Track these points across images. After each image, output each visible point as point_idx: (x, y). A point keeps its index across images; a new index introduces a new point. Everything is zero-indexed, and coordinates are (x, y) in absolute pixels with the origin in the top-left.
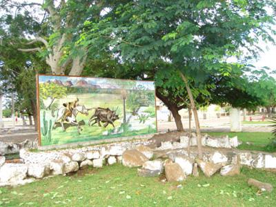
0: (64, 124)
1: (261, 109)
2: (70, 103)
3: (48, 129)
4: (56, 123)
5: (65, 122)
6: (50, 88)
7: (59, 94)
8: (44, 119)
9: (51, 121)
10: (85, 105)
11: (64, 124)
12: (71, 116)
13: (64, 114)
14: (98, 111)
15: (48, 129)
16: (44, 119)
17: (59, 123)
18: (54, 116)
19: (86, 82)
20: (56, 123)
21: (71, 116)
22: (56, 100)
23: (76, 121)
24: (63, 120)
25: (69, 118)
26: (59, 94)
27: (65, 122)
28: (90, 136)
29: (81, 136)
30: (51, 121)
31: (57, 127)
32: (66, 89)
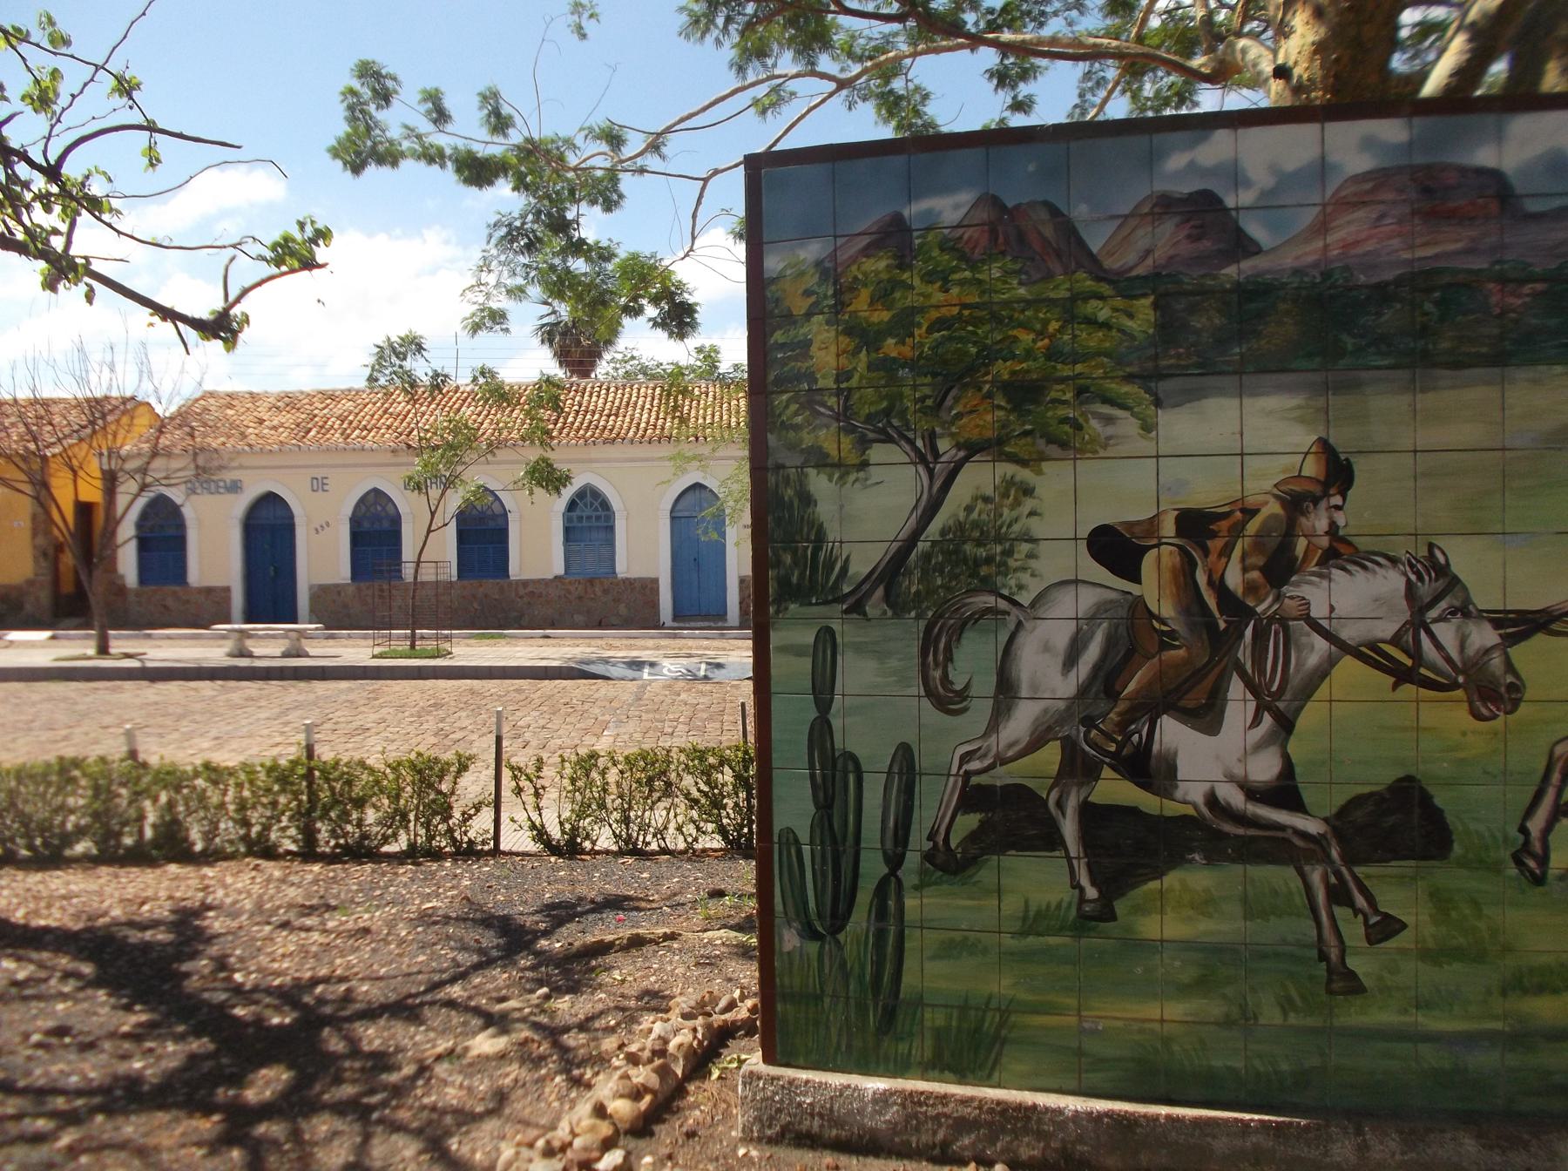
0: (1092, 815)
1: (478, 1156)
2: (1195, 524)
3: (873, 866)
4: (973, 797)
5: (1113, 789)
6: (903, 324)
7: (1023, 394)
8: (821, 730)
9: (905, 764)
10: (1463, 558)
11: (1092, 815)
12: (1207, 717)
13: (1106, 680)
14: (1516, 704)
15: (873, 866)
16: (821, 730)
17: (1019, 795)
18: (948, 700)
19: (1496, 186)
20: (973, 797)
21: (1207, 717)
22: (978, 478)
23: (1285, 793)
24: (1078, 768)
25: (1172, 733)
26: (1023, 394)
27: (1113, 789)
28: (1521, 1038)
29: (1354, 1015)
30: (905, 764)
31: (986, 843)
32: (1142, 317)
